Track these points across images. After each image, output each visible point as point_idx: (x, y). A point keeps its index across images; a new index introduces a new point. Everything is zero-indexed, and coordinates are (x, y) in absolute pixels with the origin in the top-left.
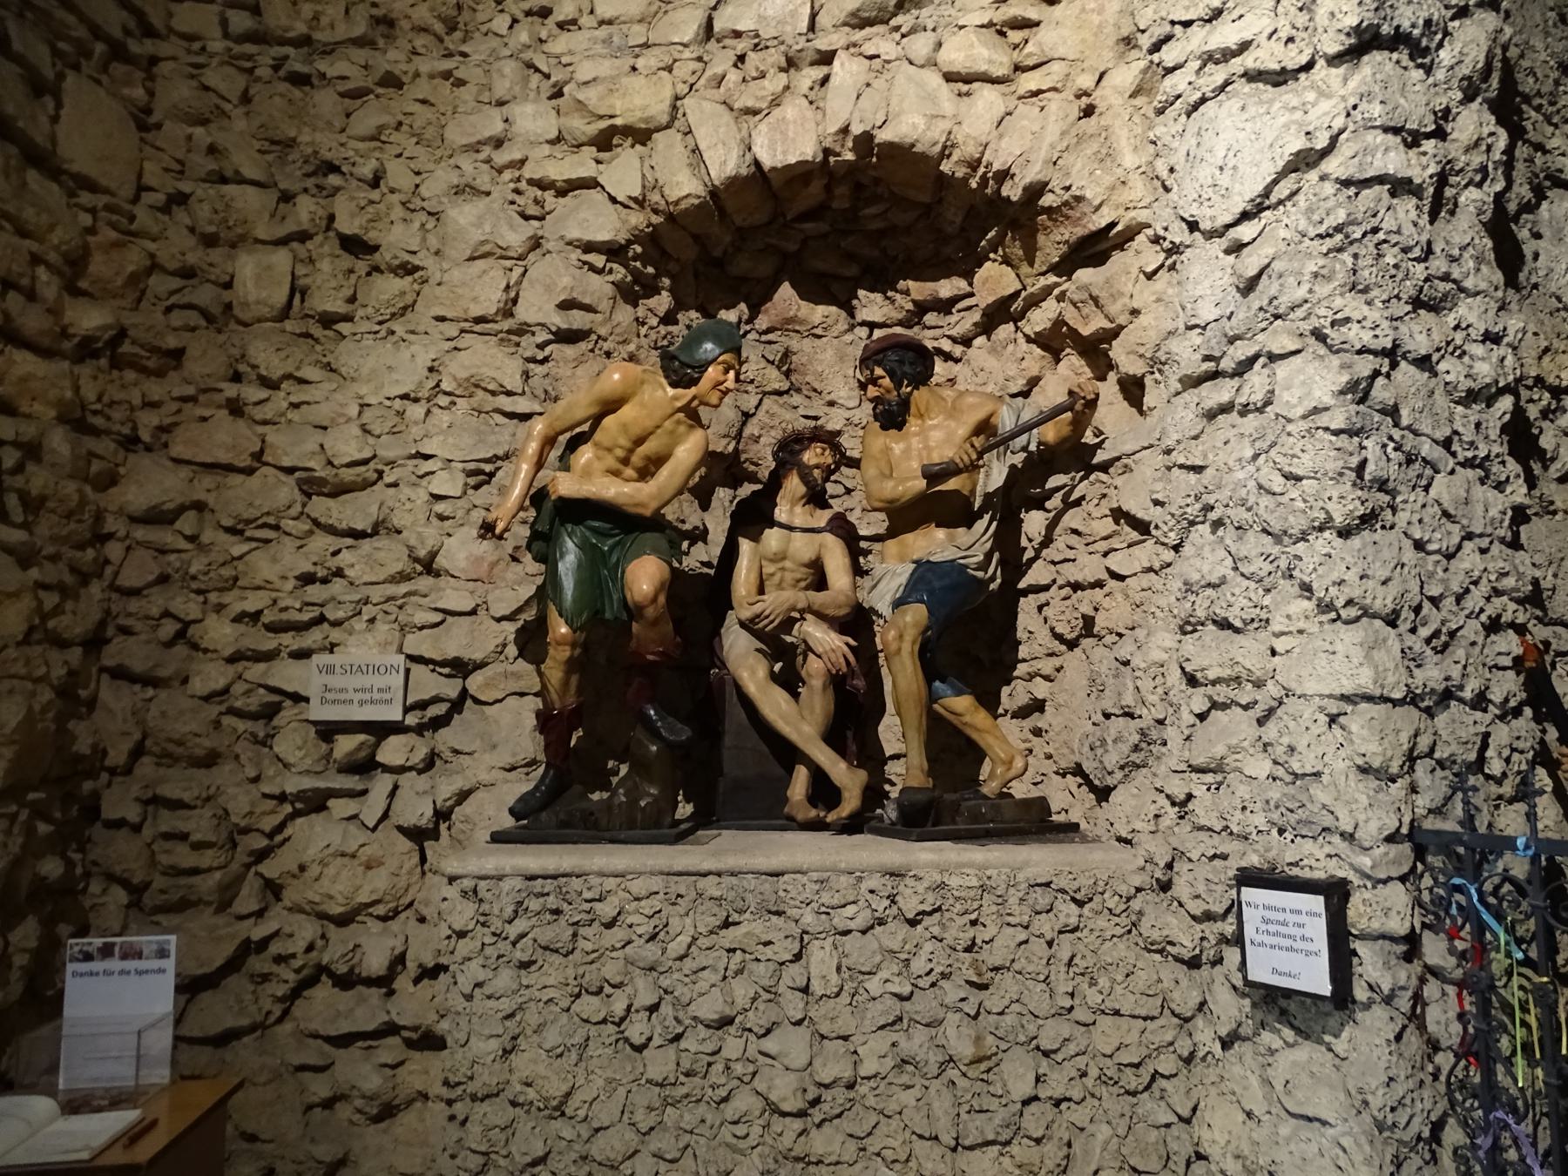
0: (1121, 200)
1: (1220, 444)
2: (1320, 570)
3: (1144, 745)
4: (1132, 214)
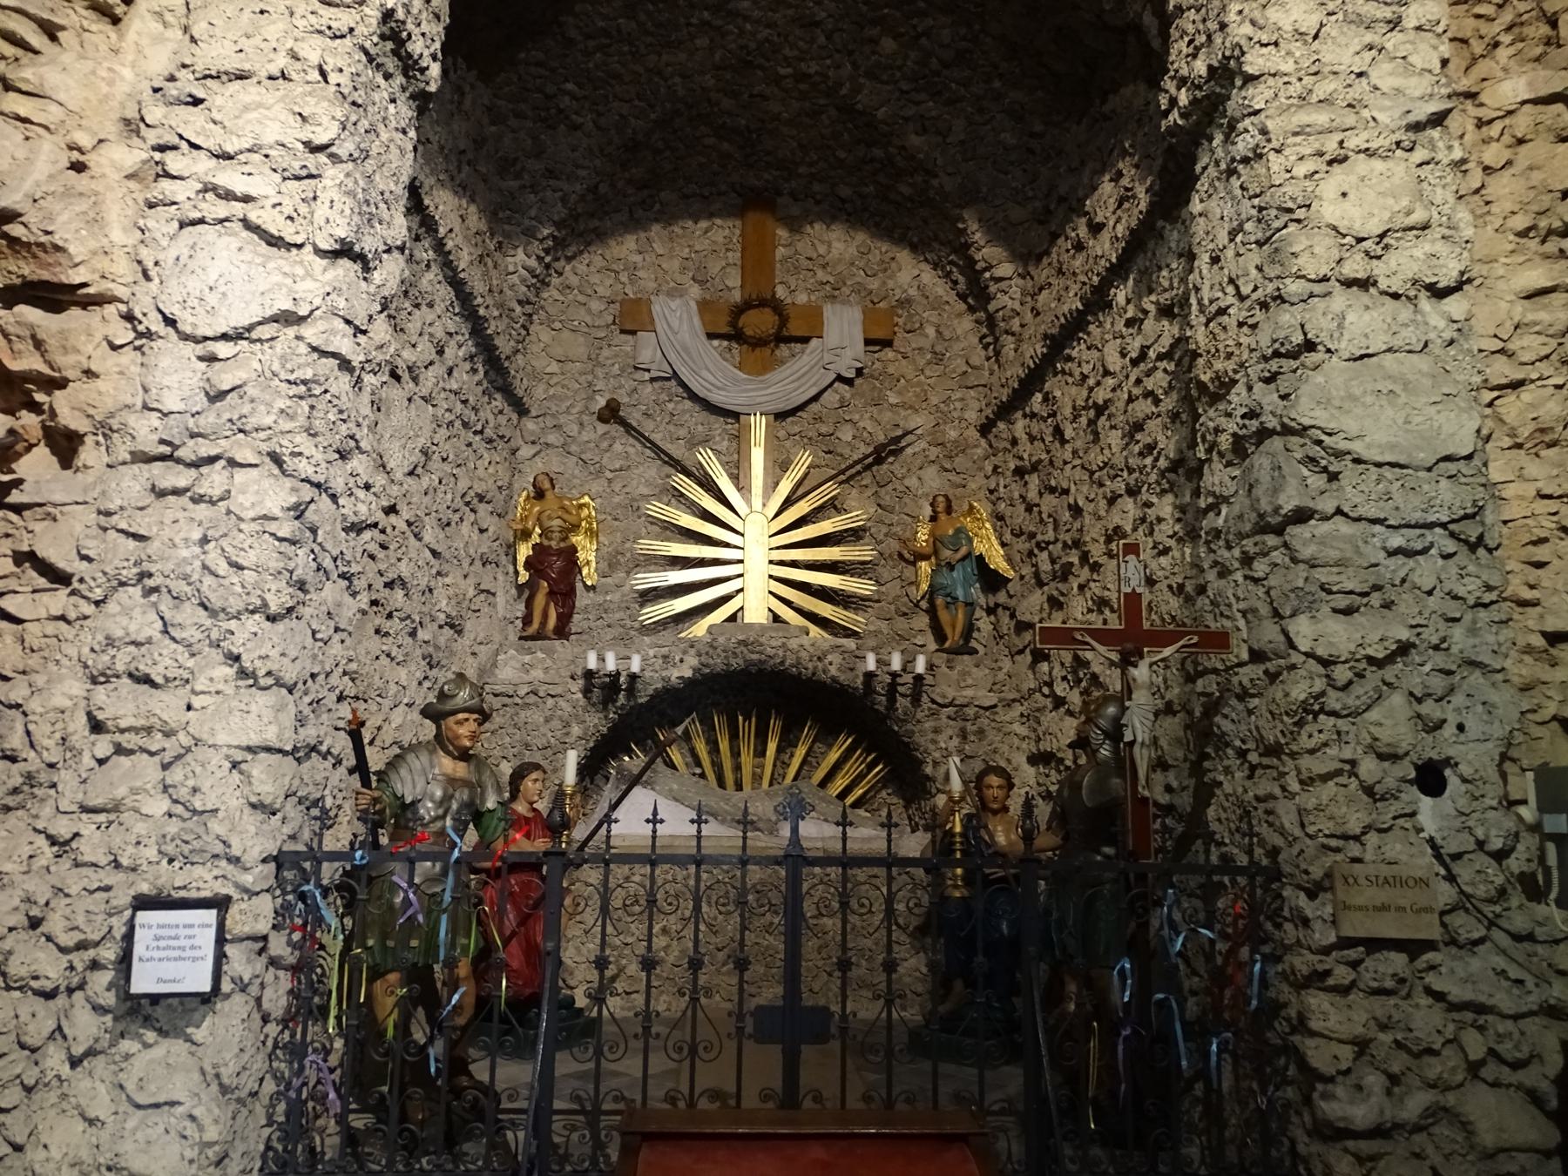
0: (99, 266)
1: (167, 521)
2: (249, 645)
3: (26, 788)
4: (111, 285)
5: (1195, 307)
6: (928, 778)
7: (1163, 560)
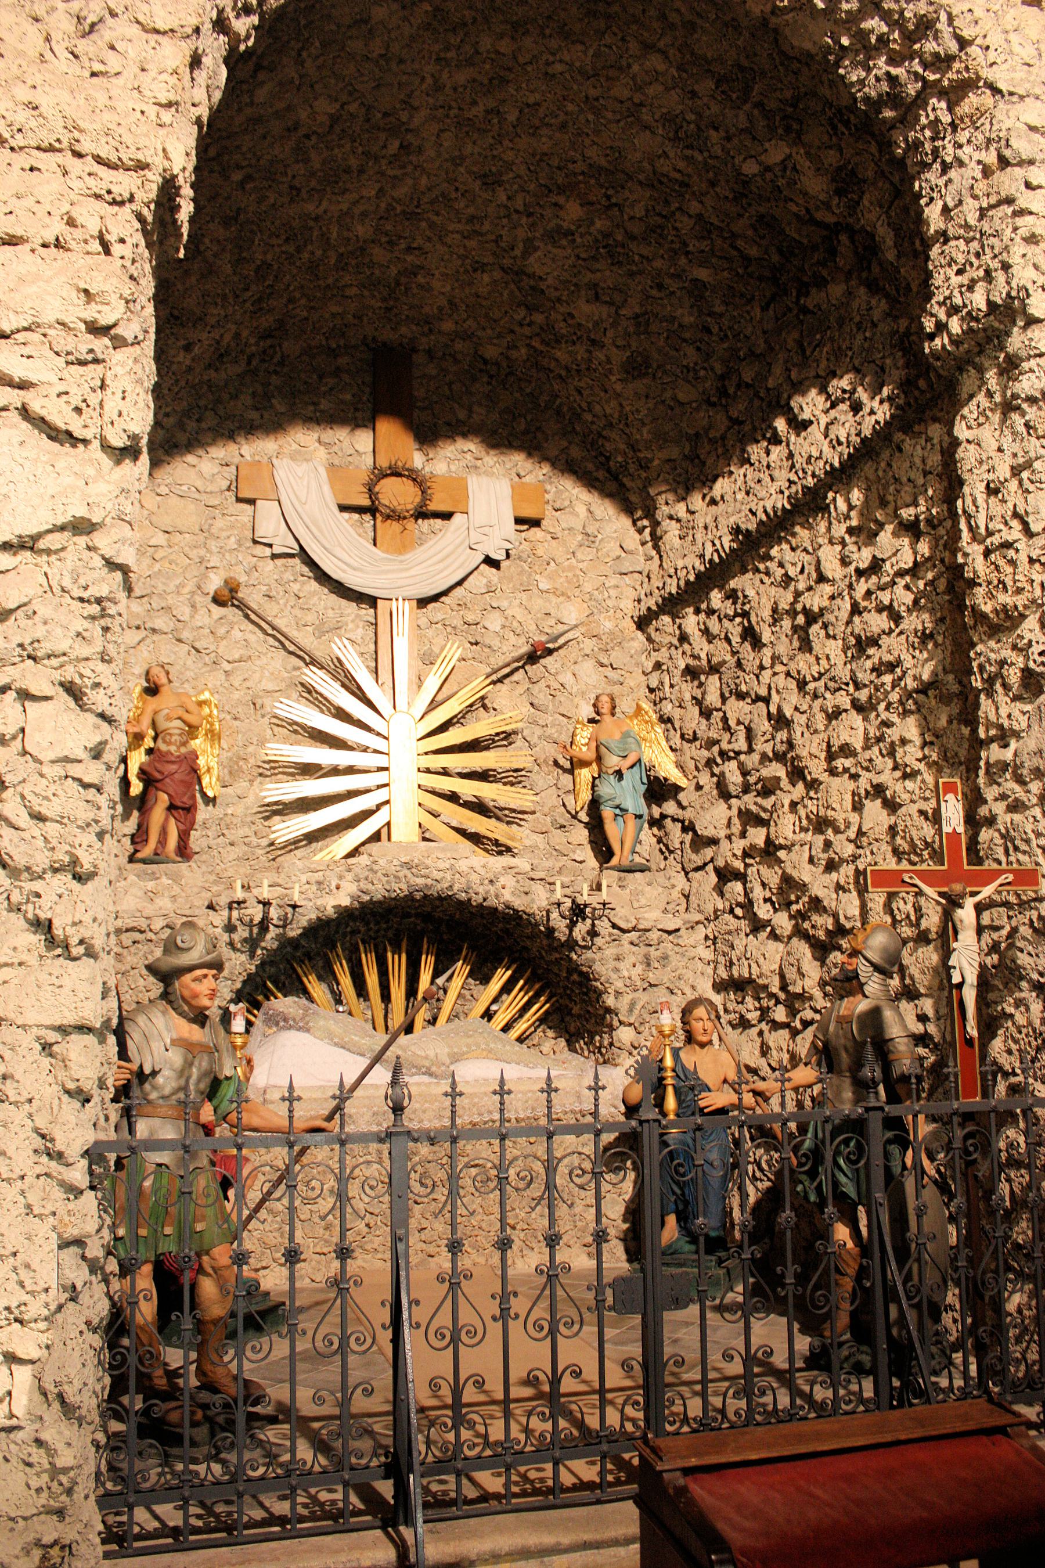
5: (965, 535)
6: (608, 1010)
7: (909, 784)
